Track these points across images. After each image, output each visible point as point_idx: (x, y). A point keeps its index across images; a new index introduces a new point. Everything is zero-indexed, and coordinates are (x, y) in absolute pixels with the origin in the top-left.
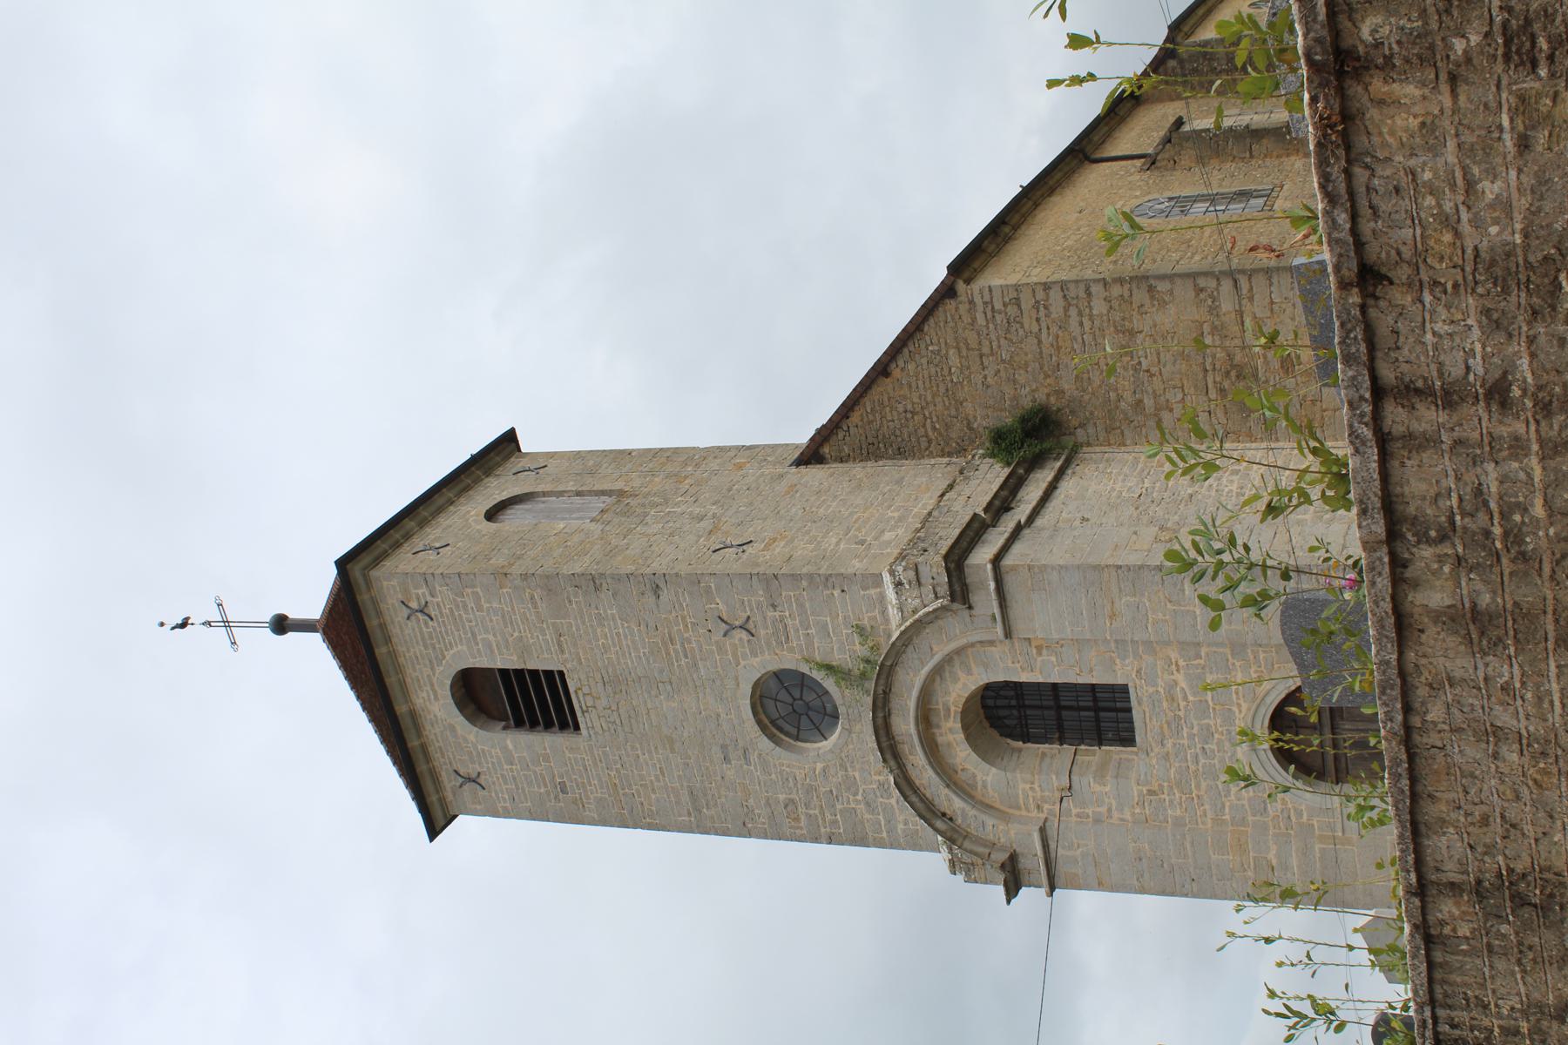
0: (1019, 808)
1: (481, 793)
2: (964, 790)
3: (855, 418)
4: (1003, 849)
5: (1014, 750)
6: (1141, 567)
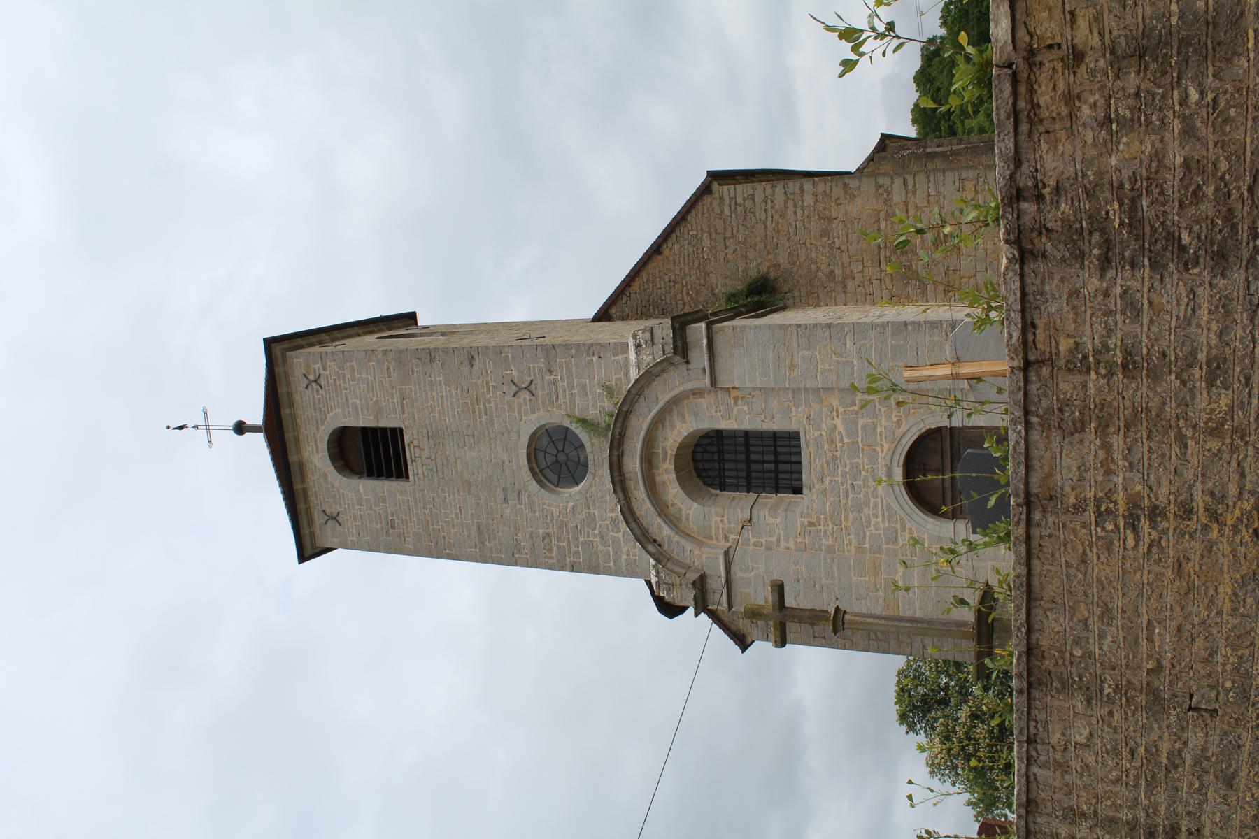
0: (711, 538)
1: (339, 529)
2: (672, 521)
3: (635, 287)
4: (696, 570)
5: (712, 495)
6: (815, 325)
